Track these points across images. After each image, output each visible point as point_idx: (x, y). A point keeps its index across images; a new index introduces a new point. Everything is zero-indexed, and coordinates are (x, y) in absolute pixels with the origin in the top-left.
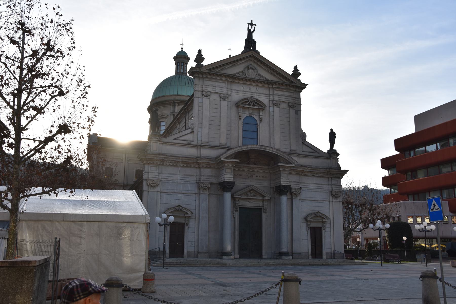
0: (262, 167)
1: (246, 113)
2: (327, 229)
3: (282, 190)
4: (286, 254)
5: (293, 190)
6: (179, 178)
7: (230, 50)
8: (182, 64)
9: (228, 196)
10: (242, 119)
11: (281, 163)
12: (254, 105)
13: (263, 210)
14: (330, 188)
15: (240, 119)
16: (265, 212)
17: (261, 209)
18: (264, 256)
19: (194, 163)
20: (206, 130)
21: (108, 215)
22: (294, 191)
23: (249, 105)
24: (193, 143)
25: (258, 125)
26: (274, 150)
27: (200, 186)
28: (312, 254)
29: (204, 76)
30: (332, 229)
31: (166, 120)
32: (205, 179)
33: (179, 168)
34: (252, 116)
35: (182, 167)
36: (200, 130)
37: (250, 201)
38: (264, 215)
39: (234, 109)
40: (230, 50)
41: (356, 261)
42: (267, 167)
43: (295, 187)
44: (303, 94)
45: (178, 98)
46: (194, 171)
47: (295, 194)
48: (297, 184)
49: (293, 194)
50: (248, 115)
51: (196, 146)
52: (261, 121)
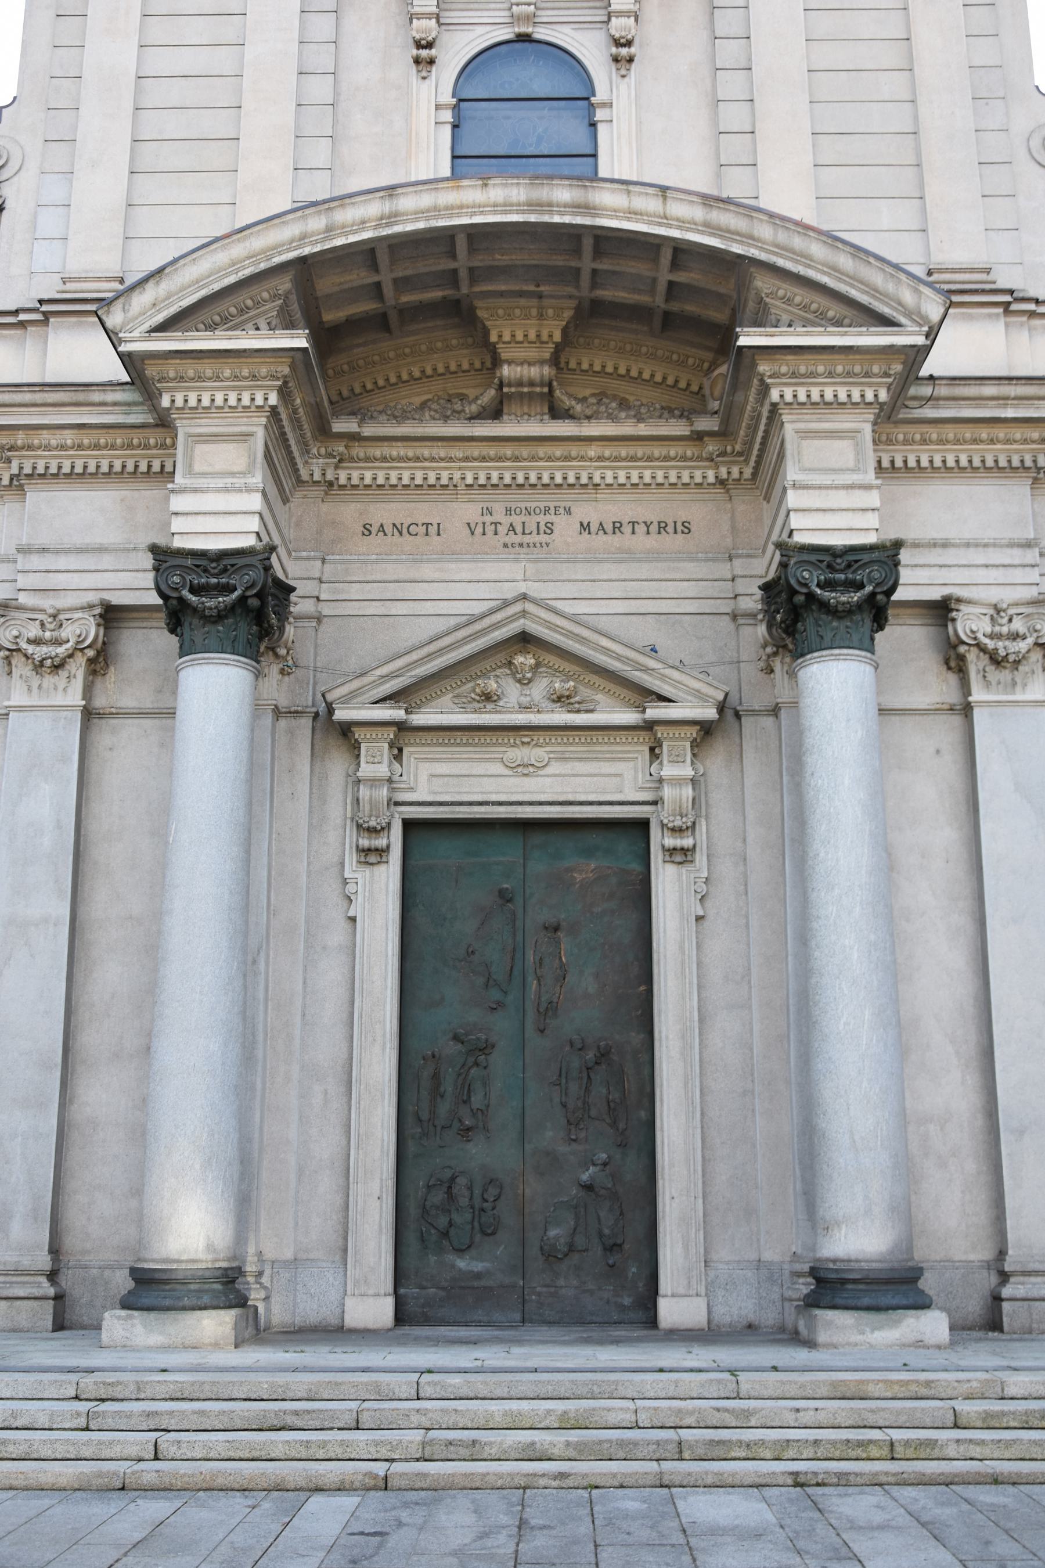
0: (628, 428)
1: (486, 17)
3: (826, 600)
4: (892, 1288)
5: (970, 623)
10: (447, 72)
11: (759, 321)
13: (658, 840)
15: (424, 64)
16: (682, 856)
17: (643, 825)
18: (671, 1311)
20: (100, 187)
21: (1005, 1220)
22: (984, 627)
25: (601, 94)
26: (678, 209)
34: (541, 33)
37: (517, 754)
38: (669, 888)
41: (867, 1013)
42: (678, 428)
43: (994, 595)
47: (997, 660)
48: (1016, 556)
49: (975, 662)
50: (505, 34)
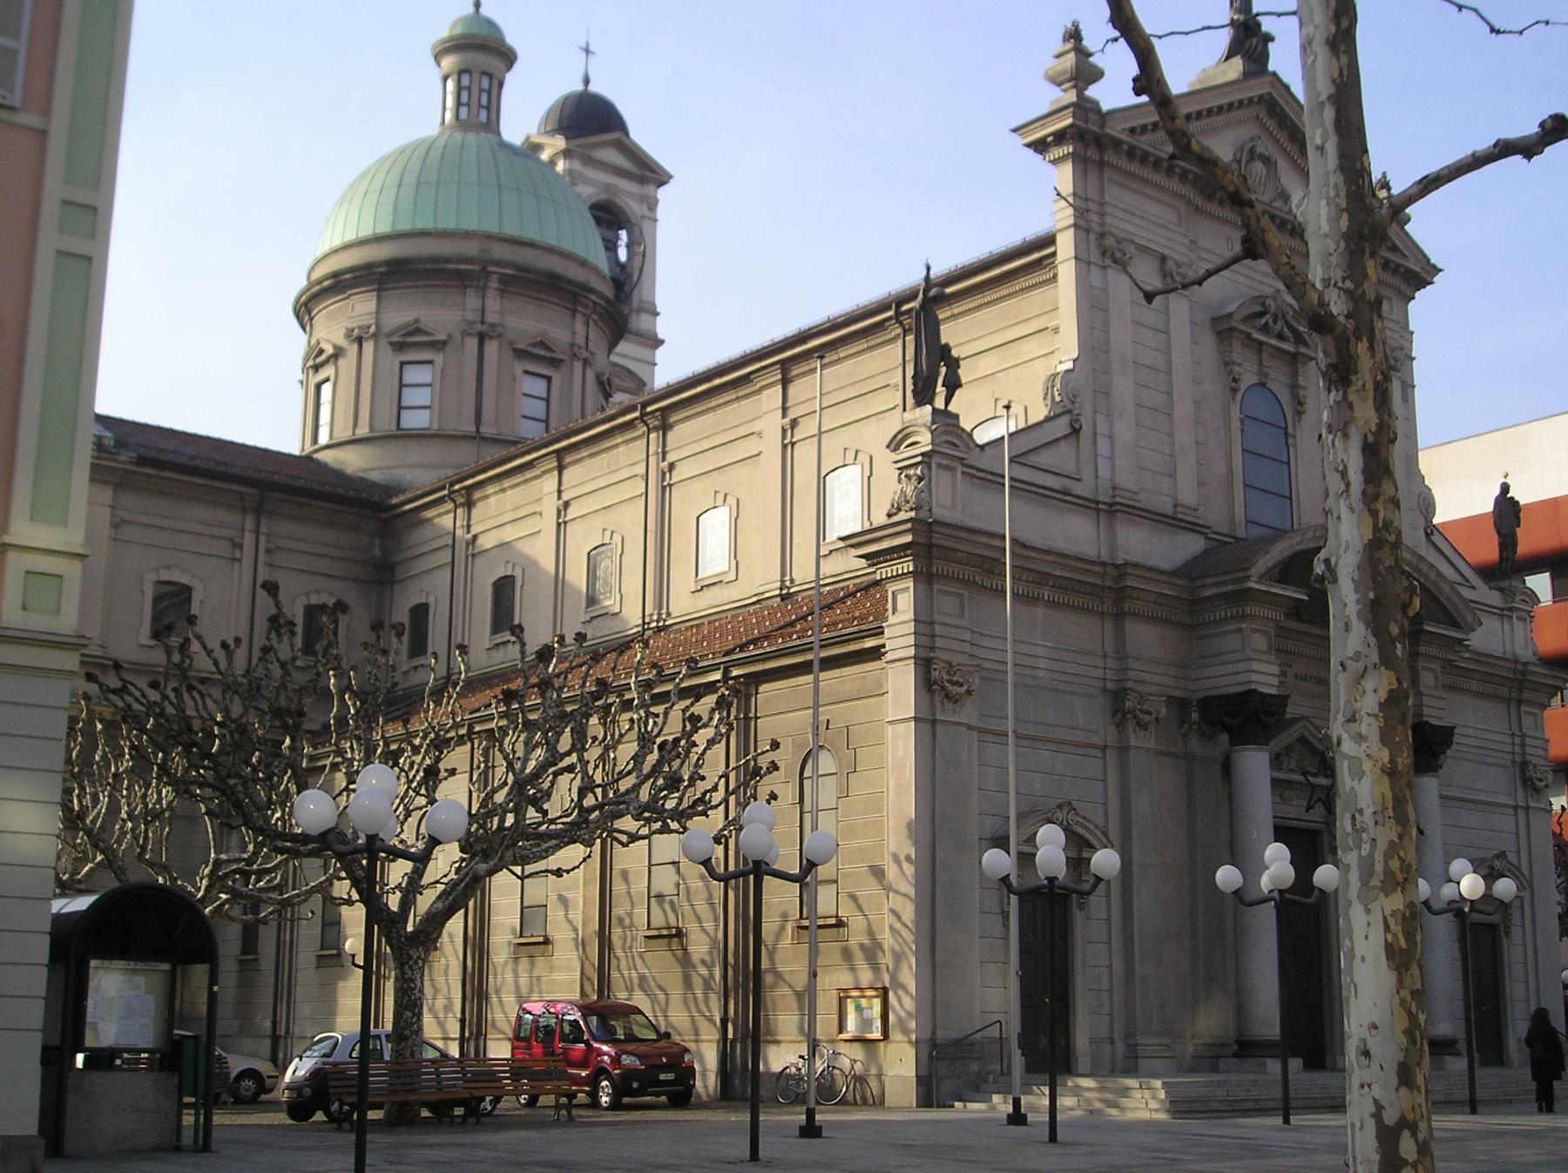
2: (1516, 932)
6: (1042, 664)
7: (587, 51)
8: (485, 84)
9: (1255, 765)
12: (1280, 337)
14: (1518, 749)
15: (1234, 391)
19: (1106, 591)
23: (1265, 329)
24: (1079, 489)
25: (1290, 431)
27: (1120, 704)
28: (1026, 1045)
29: (1109, 157)
30: (1529, 935)
31: (439, 358)
32: (1147, 677)
33: (1040, 612)
35: (1052, 604)
36: (1102, 427)
39: (1209, 341)
40: (587, 51)
44: (1423, 310)
45: (500, 252)
46: (1085, 632)
51: (1091, 506)
52: (1299, 413)
